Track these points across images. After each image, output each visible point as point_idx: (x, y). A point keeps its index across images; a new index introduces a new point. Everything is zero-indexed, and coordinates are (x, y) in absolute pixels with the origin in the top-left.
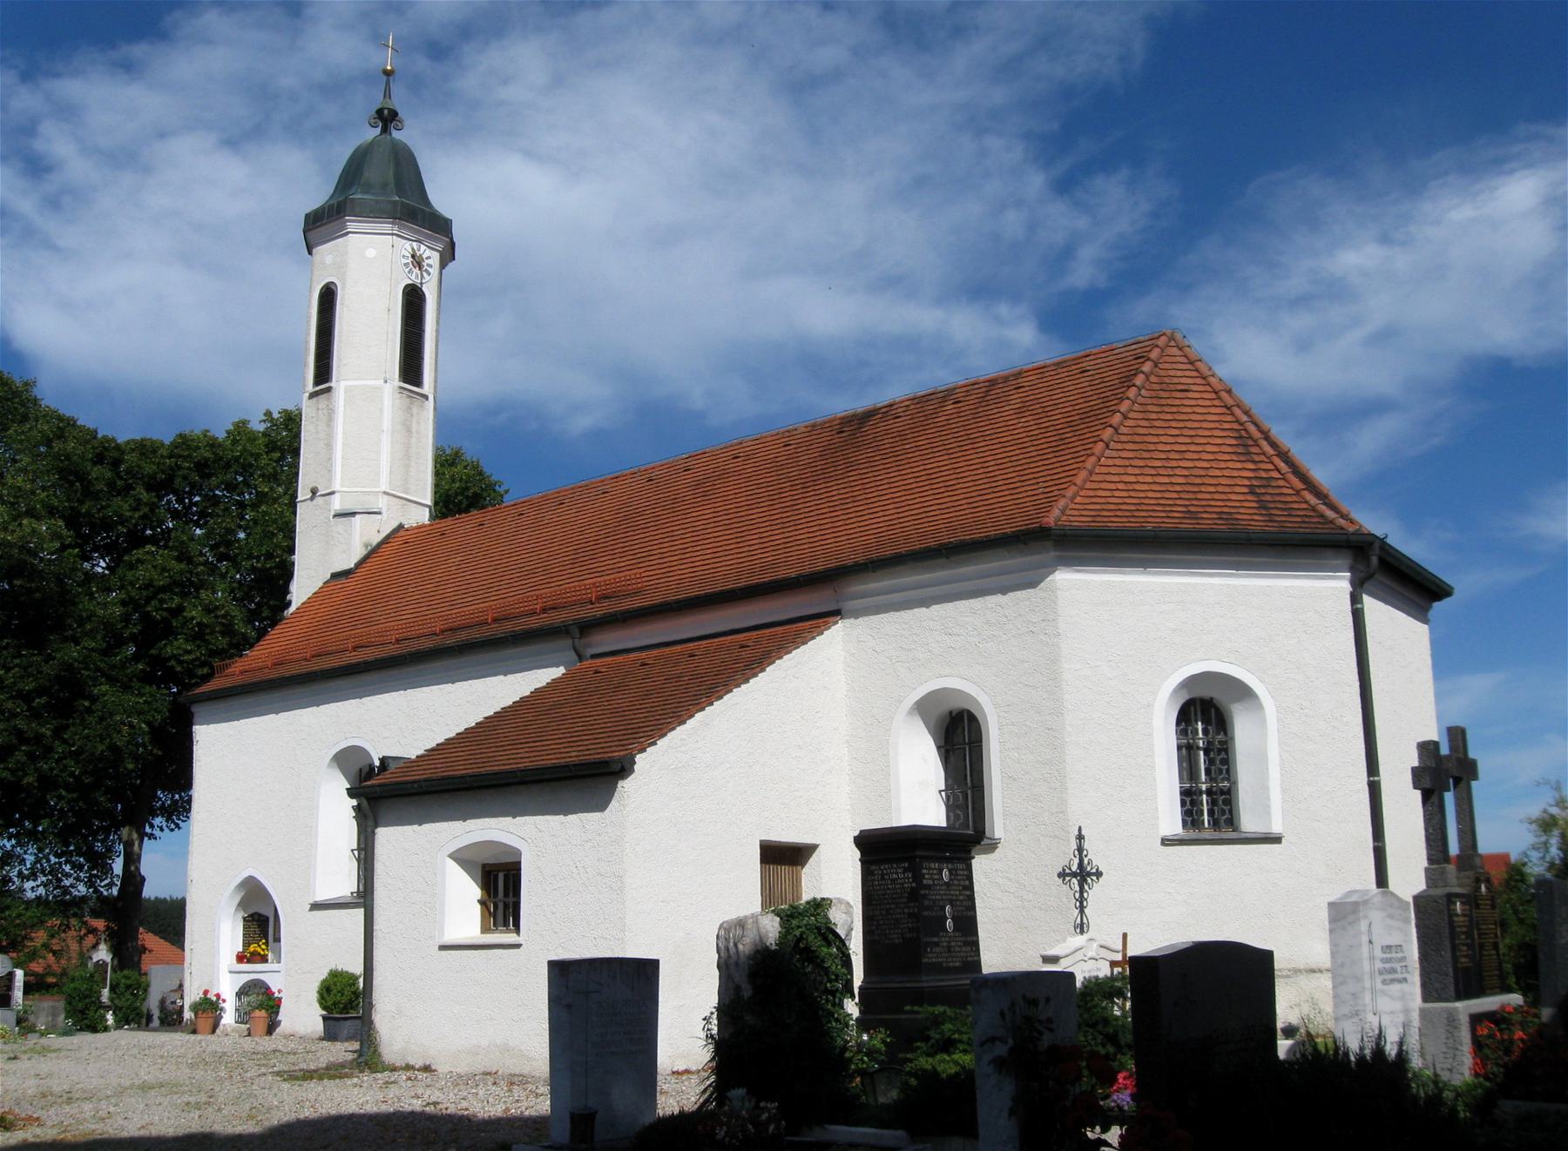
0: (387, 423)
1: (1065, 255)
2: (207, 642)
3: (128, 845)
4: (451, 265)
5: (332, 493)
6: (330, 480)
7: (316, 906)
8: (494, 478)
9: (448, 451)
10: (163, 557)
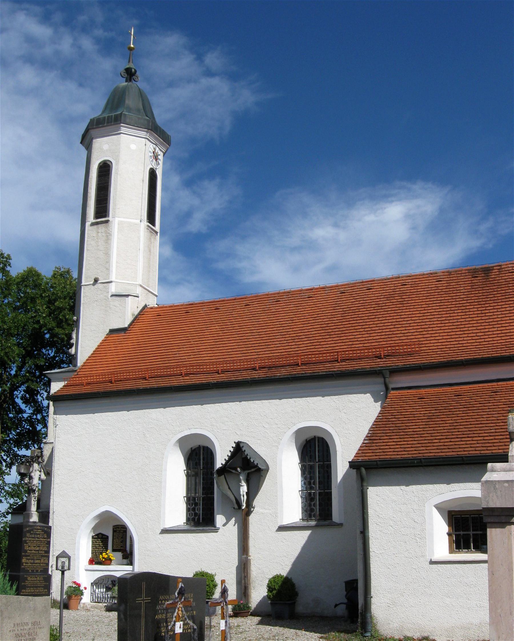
0: (142, 247)
1: (188, 215)
5: (111, 282)
6: (108, 275)
7: (165, 531)
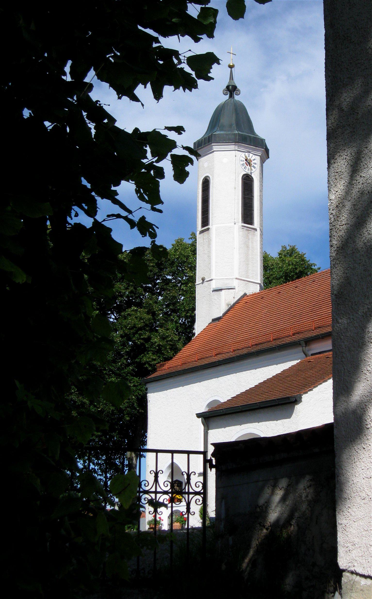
2: (163, 354)
3: (130, 459)
4: (268, 161)
8: (311, 262)
9: (288, 248)
10: (142, 313)
